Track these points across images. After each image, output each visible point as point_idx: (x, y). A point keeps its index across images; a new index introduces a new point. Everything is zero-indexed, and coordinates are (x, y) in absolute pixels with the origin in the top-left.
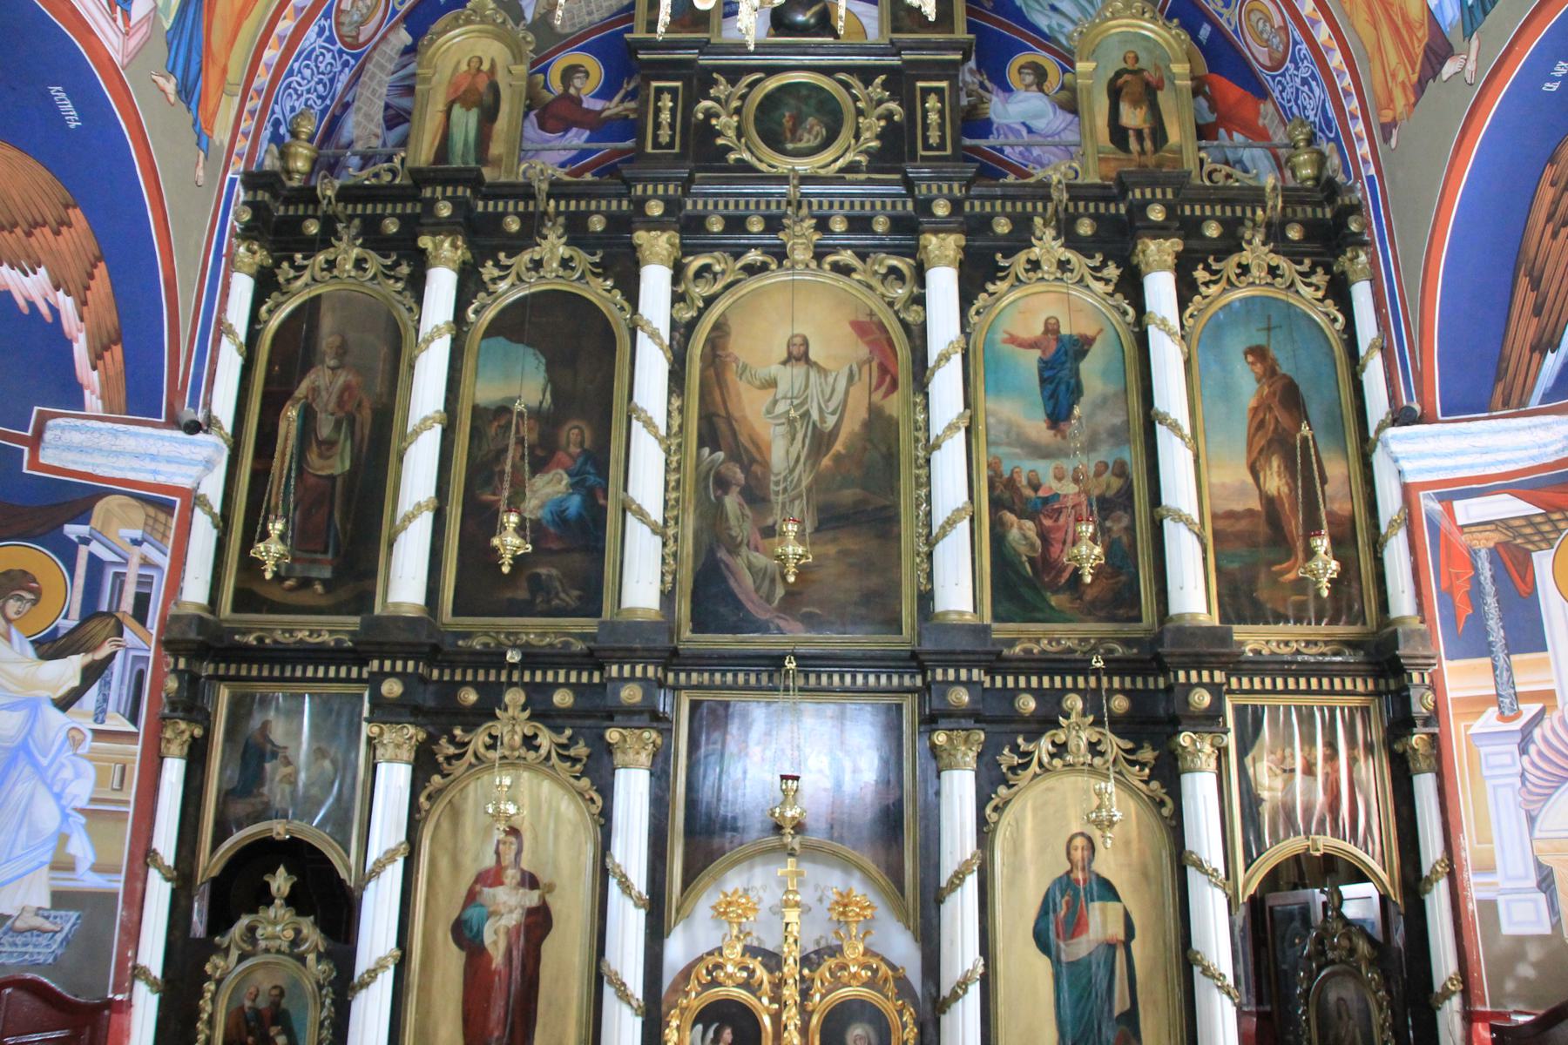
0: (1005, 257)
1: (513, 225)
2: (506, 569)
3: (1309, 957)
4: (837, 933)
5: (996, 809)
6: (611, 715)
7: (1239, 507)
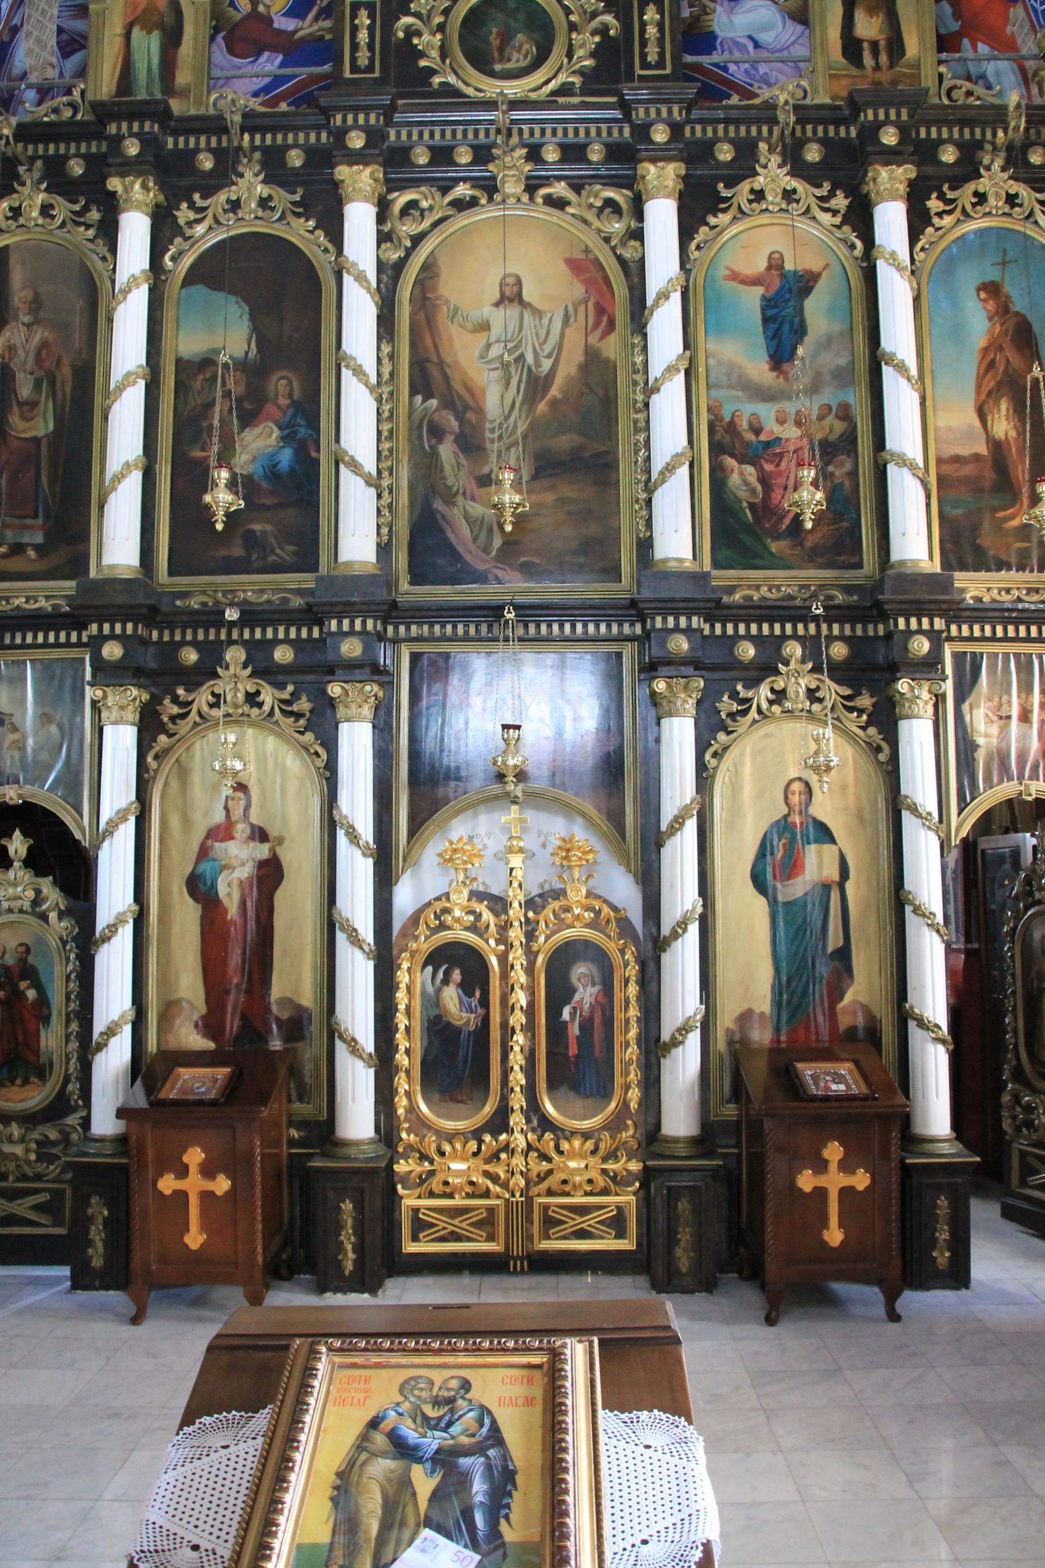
0: (728, 186)
1: (206, 162)
2: (219, 527)
3: (1017, 898)
4: (560, 877)
5: (715, 755)
6: (330, 670)
7: (964, 451)
